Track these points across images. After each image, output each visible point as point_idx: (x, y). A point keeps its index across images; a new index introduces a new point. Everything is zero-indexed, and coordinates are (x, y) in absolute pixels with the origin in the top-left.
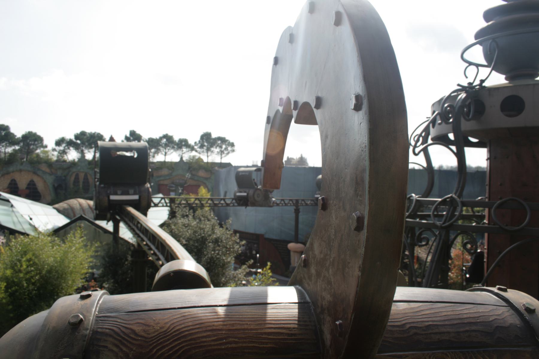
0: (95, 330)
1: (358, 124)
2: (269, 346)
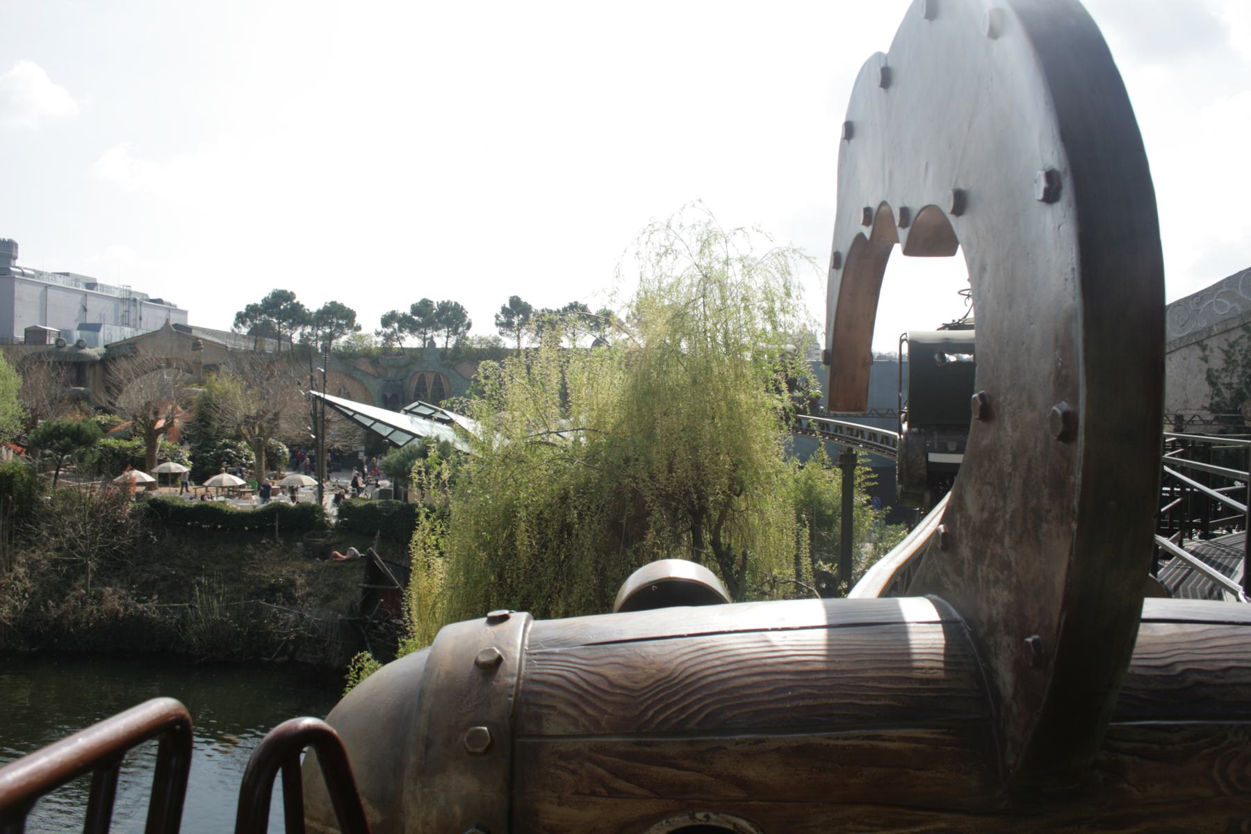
0: (528, 677)
1: (1054, 228)
2: (882, 702)
